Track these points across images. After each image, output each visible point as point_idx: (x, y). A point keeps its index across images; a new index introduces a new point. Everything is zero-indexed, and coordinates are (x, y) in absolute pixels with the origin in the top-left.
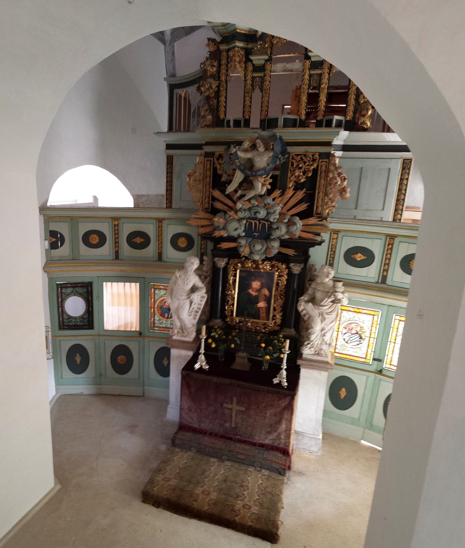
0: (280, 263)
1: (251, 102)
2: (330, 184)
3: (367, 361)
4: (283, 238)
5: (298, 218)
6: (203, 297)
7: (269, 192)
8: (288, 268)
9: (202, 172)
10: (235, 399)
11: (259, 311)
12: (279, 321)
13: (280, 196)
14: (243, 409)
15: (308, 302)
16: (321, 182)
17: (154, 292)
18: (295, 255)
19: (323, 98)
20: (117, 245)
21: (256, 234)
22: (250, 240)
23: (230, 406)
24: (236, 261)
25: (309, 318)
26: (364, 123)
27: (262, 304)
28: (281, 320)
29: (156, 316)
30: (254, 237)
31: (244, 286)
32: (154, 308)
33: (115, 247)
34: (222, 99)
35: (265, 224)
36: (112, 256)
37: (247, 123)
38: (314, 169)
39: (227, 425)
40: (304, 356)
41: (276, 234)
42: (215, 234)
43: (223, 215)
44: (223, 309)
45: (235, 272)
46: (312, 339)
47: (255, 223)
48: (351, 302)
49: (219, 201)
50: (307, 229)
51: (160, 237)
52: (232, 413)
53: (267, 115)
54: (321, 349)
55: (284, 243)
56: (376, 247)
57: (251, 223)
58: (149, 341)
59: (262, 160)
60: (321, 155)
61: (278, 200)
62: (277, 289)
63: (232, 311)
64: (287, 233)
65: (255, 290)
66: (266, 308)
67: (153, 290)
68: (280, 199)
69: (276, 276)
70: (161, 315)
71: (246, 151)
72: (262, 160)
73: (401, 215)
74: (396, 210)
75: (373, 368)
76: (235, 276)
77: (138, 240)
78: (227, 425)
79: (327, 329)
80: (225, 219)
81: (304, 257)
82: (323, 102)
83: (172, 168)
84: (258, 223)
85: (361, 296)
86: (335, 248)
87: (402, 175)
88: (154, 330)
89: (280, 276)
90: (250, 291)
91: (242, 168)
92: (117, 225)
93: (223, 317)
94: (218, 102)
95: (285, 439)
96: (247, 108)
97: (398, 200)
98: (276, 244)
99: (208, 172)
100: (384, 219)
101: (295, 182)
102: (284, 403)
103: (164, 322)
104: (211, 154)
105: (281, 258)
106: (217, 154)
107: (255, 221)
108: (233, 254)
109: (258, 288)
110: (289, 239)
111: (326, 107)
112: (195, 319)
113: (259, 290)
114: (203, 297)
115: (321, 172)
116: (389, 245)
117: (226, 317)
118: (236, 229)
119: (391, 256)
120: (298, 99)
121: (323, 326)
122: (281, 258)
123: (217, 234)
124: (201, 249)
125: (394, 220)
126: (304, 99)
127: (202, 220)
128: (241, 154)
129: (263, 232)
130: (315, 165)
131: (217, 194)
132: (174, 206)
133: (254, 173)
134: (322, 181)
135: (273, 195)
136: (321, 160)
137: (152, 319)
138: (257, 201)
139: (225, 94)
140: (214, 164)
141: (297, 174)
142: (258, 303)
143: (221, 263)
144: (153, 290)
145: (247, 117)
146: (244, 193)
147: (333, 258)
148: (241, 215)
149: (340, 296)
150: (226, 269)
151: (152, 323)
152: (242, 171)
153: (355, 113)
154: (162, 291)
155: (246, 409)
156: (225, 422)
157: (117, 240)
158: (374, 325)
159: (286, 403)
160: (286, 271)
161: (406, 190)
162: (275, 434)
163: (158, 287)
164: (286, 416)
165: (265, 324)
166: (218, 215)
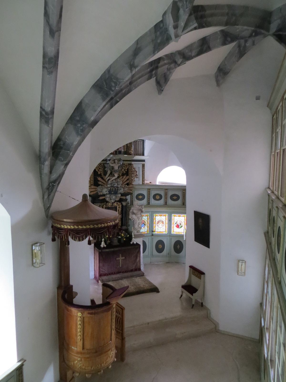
3: (148, 233)
7: (118, 177)
8: (122, 204)
10: (120, 255)
14: (124, 258)
16: (130, 172)
25: (134, 220)
30: (111, 194)
41: (119, 192)
43: (101, 187)
47: (113, 188)
49: (100, 181)
54: (138, 230)
55: (122, 195)
56: (145, 193)
57: (116, 188)
68: (122, 179)
73: (144, 182)
78: (118, 267)
80: (102, 188)
89: (119, 207)
98: (120, 195)
100: (140, 184)
101: (122, 173)
110: (124, 193)
116: (149, 192)
118: (106, 191)
123: (100, 194)
127: (92, 189)
129: (113, 191)
131: (99, 179)
136: (129, 166)
148: (109, 186)
149: (143, 210)
153: (127, 149)
155: (125, 258)
158: (148, 219)
160: (121, 206)
162: (135, 264)
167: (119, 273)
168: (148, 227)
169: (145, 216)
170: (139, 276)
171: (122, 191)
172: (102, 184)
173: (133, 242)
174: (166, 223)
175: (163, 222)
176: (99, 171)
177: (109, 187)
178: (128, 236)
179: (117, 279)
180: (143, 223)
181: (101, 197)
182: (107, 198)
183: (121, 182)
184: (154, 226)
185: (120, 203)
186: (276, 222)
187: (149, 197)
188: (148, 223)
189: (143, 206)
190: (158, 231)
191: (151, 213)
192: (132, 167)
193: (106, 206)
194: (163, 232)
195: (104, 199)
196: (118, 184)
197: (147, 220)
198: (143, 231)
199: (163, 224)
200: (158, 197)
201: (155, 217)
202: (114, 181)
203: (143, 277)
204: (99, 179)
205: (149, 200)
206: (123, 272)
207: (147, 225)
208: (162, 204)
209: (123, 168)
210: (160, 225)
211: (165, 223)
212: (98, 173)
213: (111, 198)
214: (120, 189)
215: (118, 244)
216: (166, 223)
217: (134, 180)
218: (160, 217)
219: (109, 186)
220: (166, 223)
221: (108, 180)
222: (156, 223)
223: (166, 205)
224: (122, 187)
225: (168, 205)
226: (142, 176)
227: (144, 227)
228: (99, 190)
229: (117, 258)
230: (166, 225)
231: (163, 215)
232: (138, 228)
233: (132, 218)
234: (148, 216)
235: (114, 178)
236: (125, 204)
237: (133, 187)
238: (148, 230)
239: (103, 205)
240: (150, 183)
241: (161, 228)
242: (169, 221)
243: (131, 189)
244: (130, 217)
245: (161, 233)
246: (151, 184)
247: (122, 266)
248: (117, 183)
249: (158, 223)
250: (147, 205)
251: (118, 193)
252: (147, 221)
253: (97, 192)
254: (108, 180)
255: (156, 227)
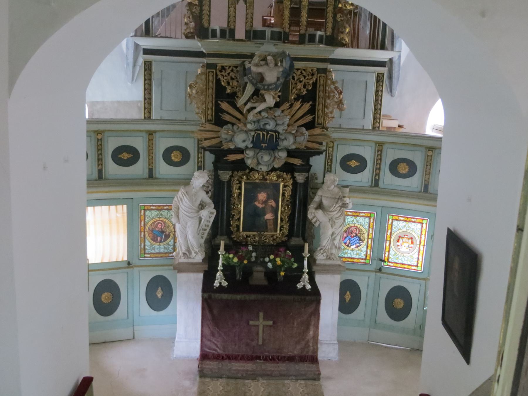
0: (285, 174)
1: (235, 13)
2: (329, 97)
3: (368, 261)
4: (290, 148)
5: (304, 129)
6: (212, 213)
7: (277, 105)
8: (293, 177)
9: (205, 84)
10: (261, 314)
11: (266, 223)
12: (286, 232)
13: (288, 109)
14: (271, 323)
15: (317, 209)
16: (320, 94)
17: (144, 214)
18: (302, 165)
19: (304, 14)
20: (100, 162)
21: (263, 145)
22: (257, 151)
23: (257, 323)
24: (240, 173)
25: (319, 225)
26: (343, 39)
27: (269, 216)
28: (289, 230)
29: (147, 241)
30: (261, 148)
31: (250, 199)
32: (144, 232)
33: (98, 165)
34: (206, 8)
35: (273, 135)
36: (146, 175)
37: (232, 32)
38: (313, 82)
39: (254, 343)
40: (317, 262)
42: (224, 147)
44: (229, 225)
45: (239, 185)
46: (324, 244)
47: (263, 135)
48: (355, 206)
49: (228, 113)
50: (312, 139)
51: (151, 151)
52: (258, 329)
53: (252, 26)
54: (332, 254)
55: (291, 154)
58: (139, 271)
59: (271, 75)
60: (318, 70)
61: (286, 112)
62: (283, 200)
63: (238, 227)
64: (295, 142)
65: (261, 202)
66: (273, 219)
67: (142, 212)
68: (289, 110)
69: (281, 186)
70: (153, 240)
71: (257, 65)
72: (271, 75)
73: (379, 123)
74: (375, 119)
75: (373, 268)
76: (240, 188)
77: (125, 156)
78: (254, 343)
79: (337, 234)
80: (233, 131)
81: (307, 167)
82: (305, 18)
83: (151, 75)
84: (266, 134)
85: (360, 199)
86: (332, 156)
87: (377, 87)
88: (145, 257)
89: (285, 186)
90: (256, 203)
91: (255, 82)
92: (101, 139)
93: (229, 233)
94: (201, 10)
95: (313, 346)
96: (231, 18)
97: (375, 110)
98: (283, 155)
99: (211, 84)
101: (297, 94)
102: (310, 309)
103: (157, 247)
104: (214, 66)
105: (288, 168)
106: (219, 67)
107: (264, 132)
108: (240, 165)
109: (264, 199)
110: (296, 149)
111: (308, 22)
112: (202, 237)
113: (265, 202)
114: (212, 213)
115: (320, 85)
117: (232, 233)
118: (244, 141)
119: (381, 161)
120: (281, 13)
121: (333, 230)
122: (288, 168)
123: (225, 146)
124: (198, 163)
125: (374, 128)
126: (287, 13)
127: (207, 133)
128: (254, 69)
129: (266, 142)
130: (315, 79)
131: (225, 106)
132: (153, 117)
133: (266, 87)
134: (321, 93)
135: (282, 108)
136: (319, 75)
137: (143, 245)
138: (267, 113)
139: (208, 3)
140: (217, 75)
141: (298, 87)
142: (265, 215)
143: (225, 176)
144: (142, 212)
145: (233, 27)
146: (254, 105)
147: (331, 166)
148: (249, 126)
149: (347, 200)
150: (229, 182)
151: (143, 250)
152: (254, 84)
153: (333, 29)
154: (153, 211)
155: (274, 323)
156: (252, 340)
157: (100, 156)
158: (371, 227)
159: (313, 308)
160: (291, 182)
161: (381, 101)
163: (149, 208)
164: (313, 323)
165: (273, 236)
166: (225, 127)
167: (252, 358)
168: (369, 248)
169: (362, 216)
170: (304, 377)
171: (289, 143)
172: (234, 120)
173: (304, 286)
174: (420, 242)
175: (412, 238)
176: (231, 84)
177: (251, 130)
178: (296, 265)
179: (239, 375)
180: (356, 235)
181: (232, 156)
182: (248, 158)
183: (287, 120)
184: (387, 248)
185: (289, 176)
186: (502, 334)
187: (378, 166)
188: (370, 237)
189: (347, 190)
190: (396, 261)
191: (380, 209)
192: (327, 78)
193: (248, 179)
194: (410, 265)
195: (242, 161)
196: (278, 122)
197: (367, 227)
198: (354, 256)
199: (412, 245)
200: (403, 169)
201: (392, 223)
202: (264, 114)
203: (316, 383)
204: (225, 106)
205: (378, 174)
206: (266, 359)
207: (366, 240)
208: (416, 190)
209: (301, 82)
210: (405, 245)
211: (418, 243)
212: (225, 88)
213: (260, 162)
214: (283, 138)
215: (265, 283)
216: (422, 243)
217: (330, 115)
218: (405, 223)
219: (249, 126)
220: (420, 242)
221: (249, 111)
222: (392, 240)
223: (426, 195)
224: (290, 133)
225: (431, 193)
226: (375, 106)
227: (358, 247)
228: (224, 136)
229: (252, 320)
230: (419, 248)
231: (413, 220)
232: (331, 249)
233: (314, 217)
234: (370, 217)
235: (261, 107)
236: (301, 178)
237: (325, 135)
238: (368, 256)
239: (242, 178)
240: (400, 126)
241: (405, 255)
242: (430, 238)
243: (319, 141)
244: (310, 216)
245: (404, 268)
246: (401, 130)
247: (263, 343)
248: (276, 121)
249: (398, 241)
250: (371, 186)
251: (279, 148)
252: (369, 231)
253: (221, 142)
254: (249, 111)
255: (391, 250)
